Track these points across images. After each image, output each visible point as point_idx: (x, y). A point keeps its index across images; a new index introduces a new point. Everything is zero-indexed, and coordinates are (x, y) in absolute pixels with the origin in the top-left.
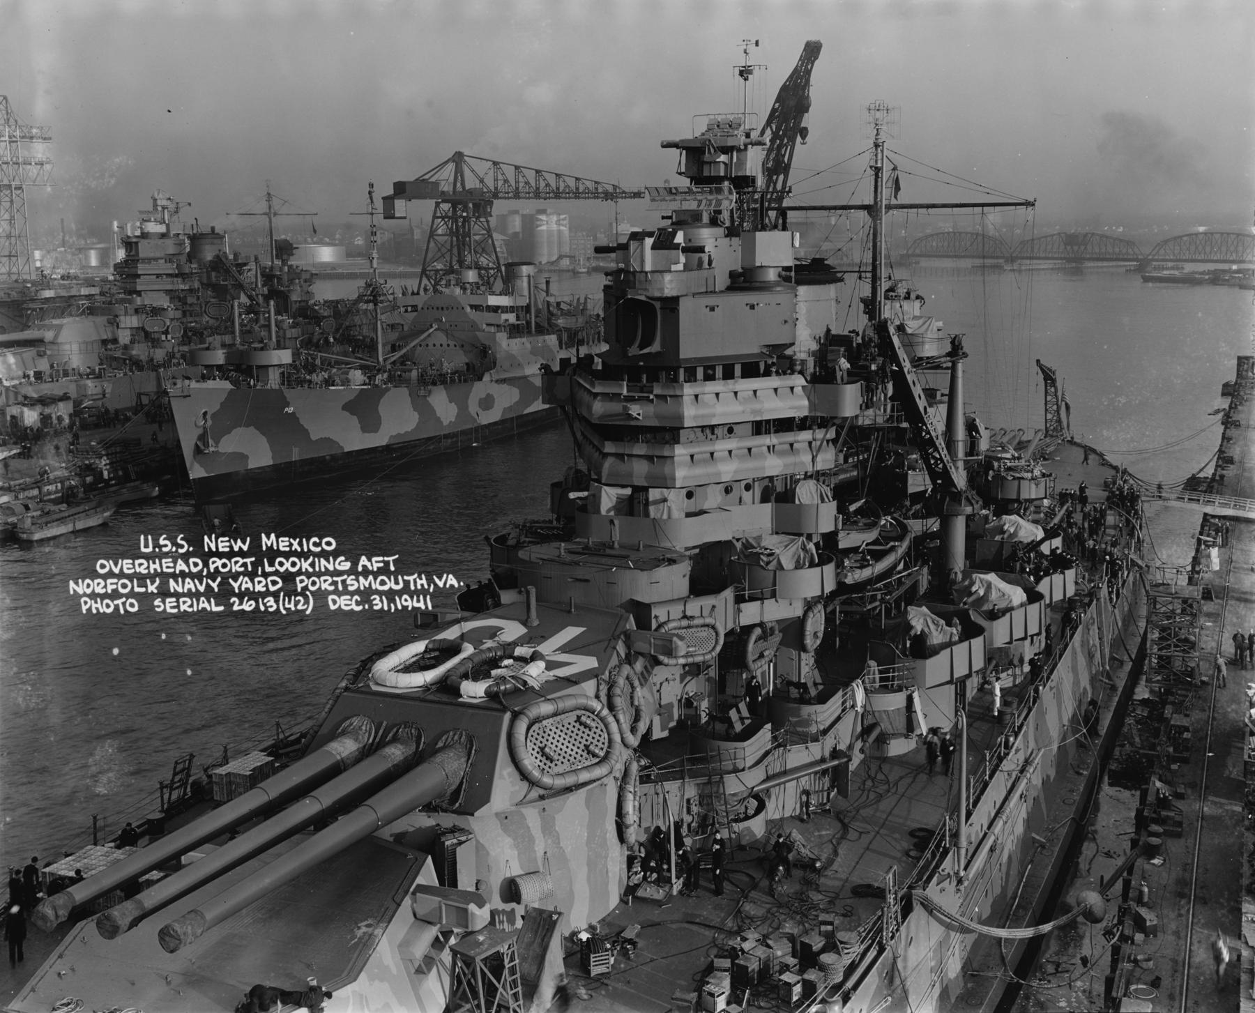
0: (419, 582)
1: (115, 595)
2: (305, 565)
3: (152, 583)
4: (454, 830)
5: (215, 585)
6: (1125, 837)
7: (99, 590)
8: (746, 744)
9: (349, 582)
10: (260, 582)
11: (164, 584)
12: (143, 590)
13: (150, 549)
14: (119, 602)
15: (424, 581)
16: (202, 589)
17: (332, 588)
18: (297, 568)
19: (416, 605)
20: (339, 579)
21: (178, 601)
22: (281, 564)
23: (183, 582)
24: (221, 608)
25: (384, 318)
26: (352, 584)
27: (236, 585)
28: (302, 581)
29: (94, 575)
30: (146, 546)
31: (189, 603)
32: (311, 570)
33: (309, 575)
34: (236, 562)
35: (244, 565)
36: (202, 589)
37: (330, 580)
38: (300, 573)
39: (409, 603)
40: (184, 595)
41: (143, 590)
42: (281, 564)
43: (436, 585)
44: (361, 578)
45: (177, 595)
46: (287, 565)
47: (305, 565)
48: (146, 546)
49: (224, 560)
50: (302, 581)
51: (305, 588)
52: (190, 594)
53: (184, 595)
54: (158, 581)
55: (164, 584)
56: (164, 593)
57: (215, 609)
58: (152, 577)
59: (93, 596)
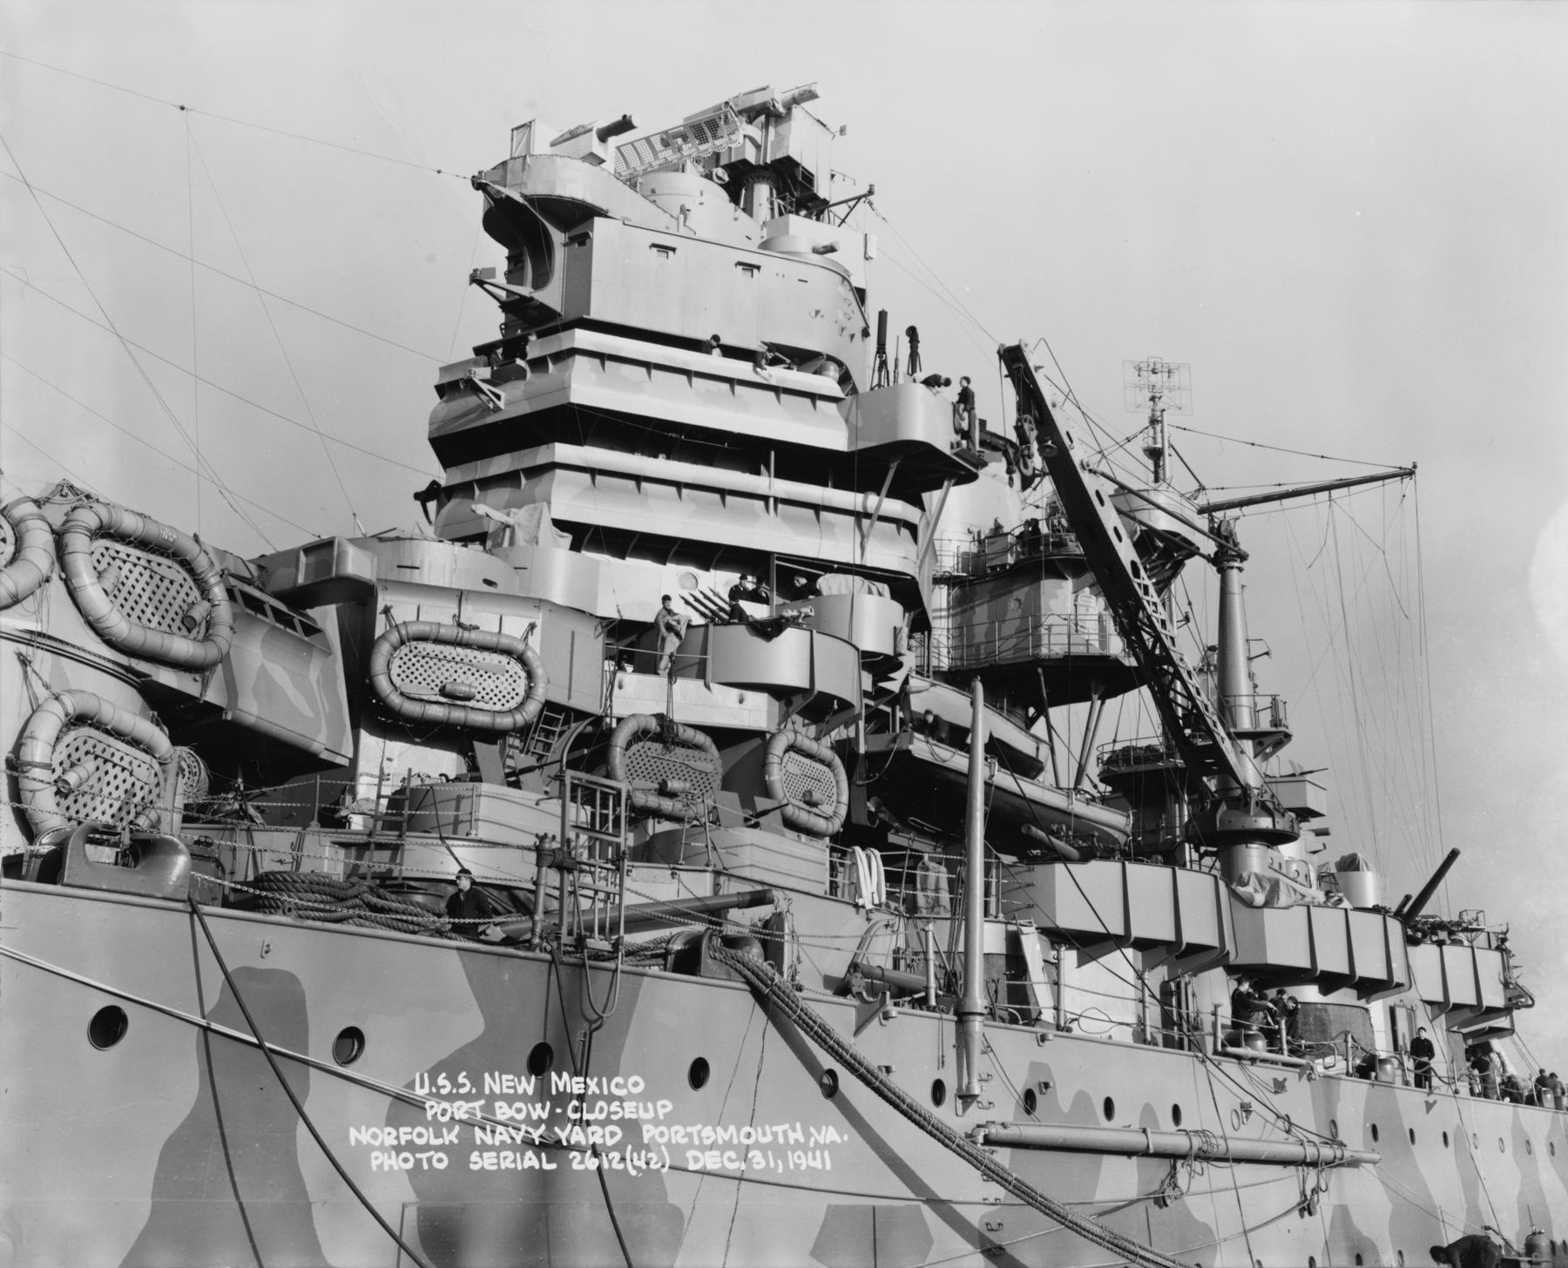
9: (704, 1134)
30: (422, 1086)
48: (422, 1086)
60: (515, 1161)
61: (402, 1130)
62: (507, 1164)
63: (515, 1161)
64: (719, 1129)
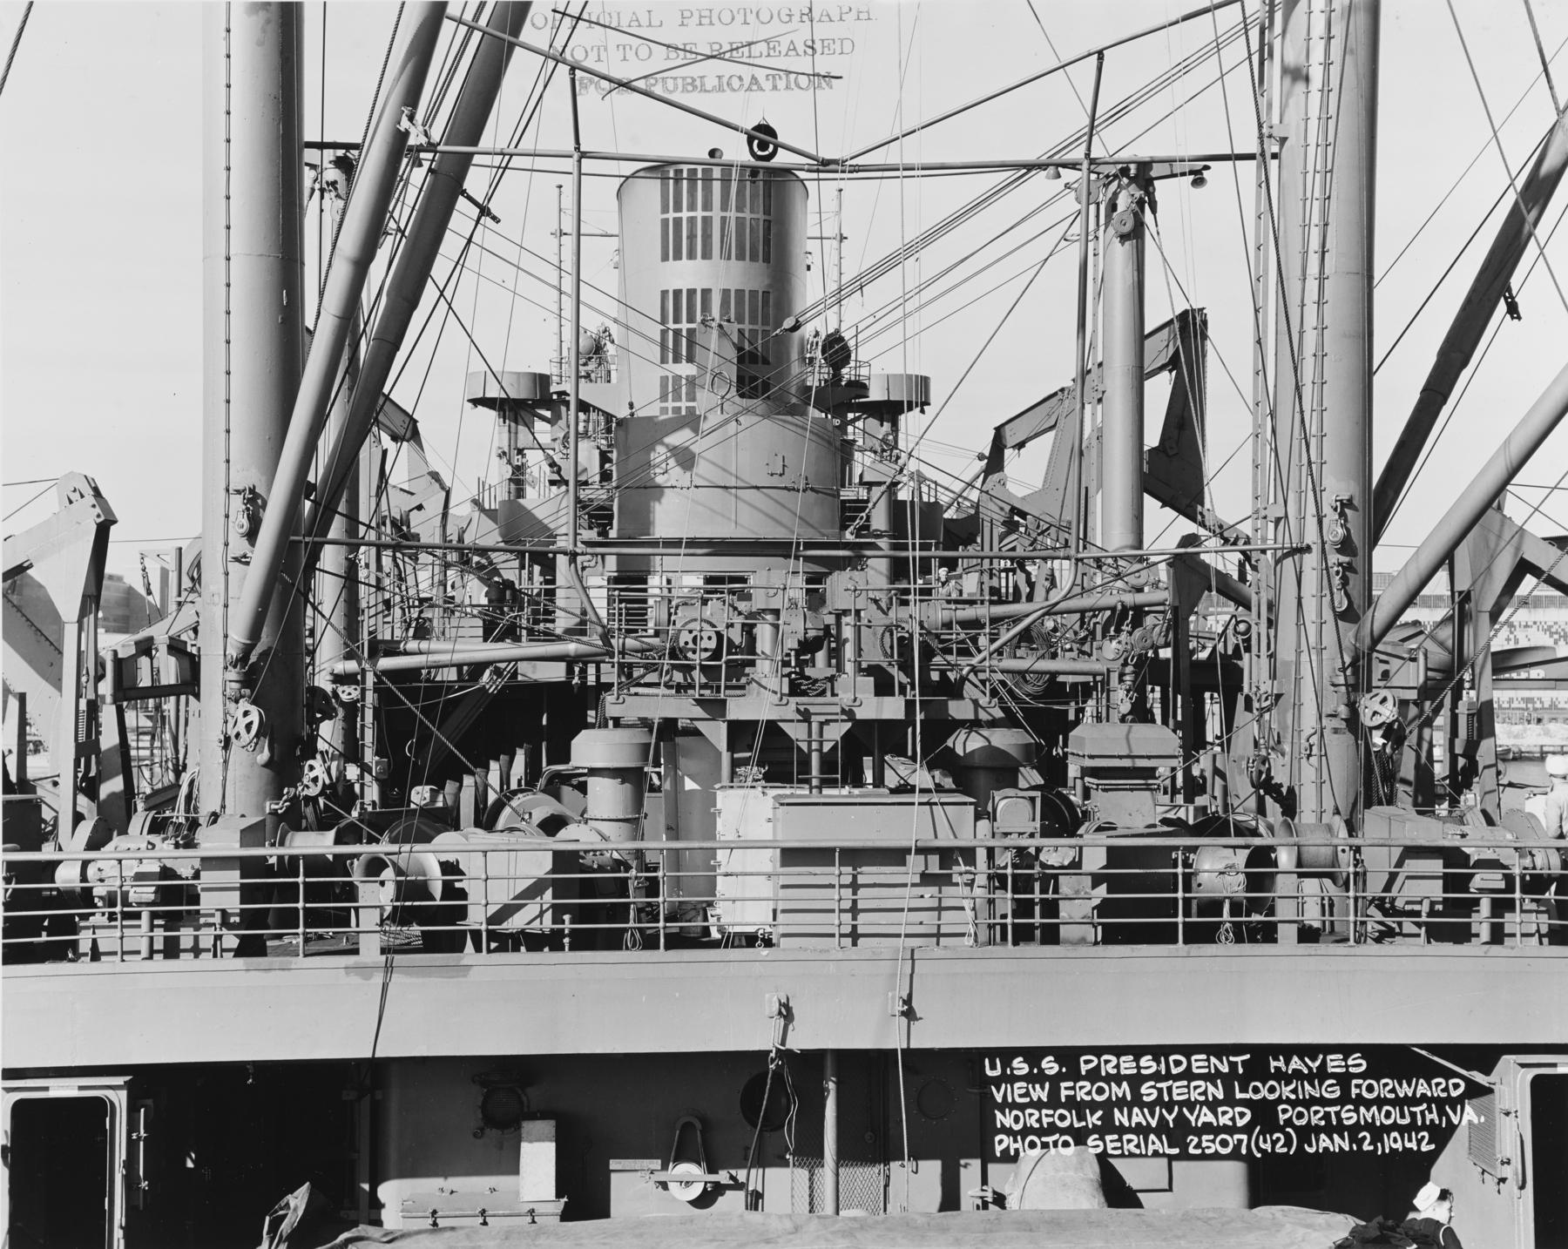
0: (1429, 1117)
2: (1286, 1091)
5: (1170, 1118)
8: (853, 357)
9: (1344, 1115)
10: (1224, 1113)
15: (1435, 1116)
16: (1154, 1123)
17: (1202, 1098)
18: (1277, 1094)
19: (1408, 1145)
21: (1120, 1140)
22: (1256, 1090)
23: (1317, 1141)
25: (1072, 552)
26: (1349, 1117)
27: (1192, 1119)
28: (1285, 1111)
30: (993, 1067)
32: (1293, 1097)
33: (1294, 1104)
34: (1316, 1112)
35: (1327, 1116)
36: (1154, 1123)
38: (1279, 1101)
39: (1398, 1146)
40: (1129, 1130)
42: (1256, 1090)
43: (1449, 1120)
44: (1362, 1110)
45: (1121, 1130)
46: (1264, 1093)
47: (1286, 1091)
48: (993, 1067)
49: (1388, 1122)
50: (1285, 1111)
51: (1289, 1122)
53: (1129, 1130)
55: (1108, 1119)
58: (1094, 1106)
60: (1138, 1146)
64: (1362, 1110)
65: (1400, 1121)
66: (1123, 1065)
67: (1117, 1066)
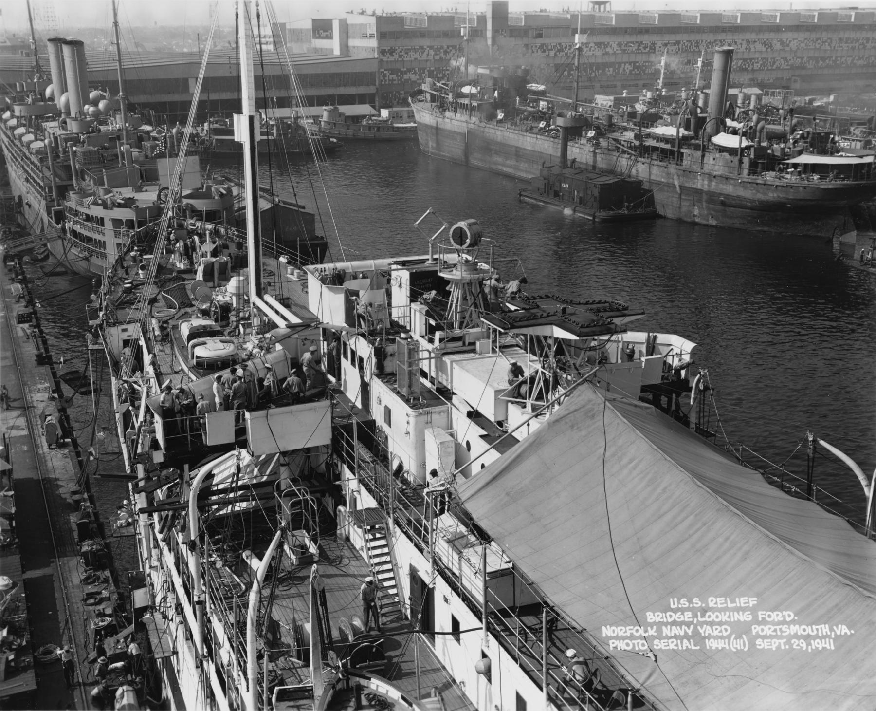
1: (632, 637)
3: (652, 629)
4: (368, 599)
6: (315, 209)
7: (621, 634)
11: (659, 631)
12: (734, 605)
13: (676, 606)
14: (635, 642)
20: (778, 627)
24: (698, 648)
27: (702, 631)
29: (667, 609)
31: (675, 643)
36: (690, 632)
37: (773, 628)
41: (734, 605)
52: (675, 637)
54: (655, 627)
56: (660, 637)
57: (693, 648)
59: (617, 638)
60: (677, 645)
61: (628, 628)
62: (672, 646)
63: (677, 645)
65: (811, 633)
66: (719, 602)
67: (716, 603)
